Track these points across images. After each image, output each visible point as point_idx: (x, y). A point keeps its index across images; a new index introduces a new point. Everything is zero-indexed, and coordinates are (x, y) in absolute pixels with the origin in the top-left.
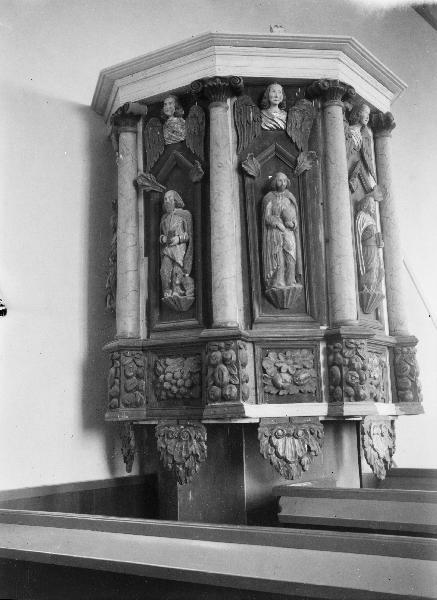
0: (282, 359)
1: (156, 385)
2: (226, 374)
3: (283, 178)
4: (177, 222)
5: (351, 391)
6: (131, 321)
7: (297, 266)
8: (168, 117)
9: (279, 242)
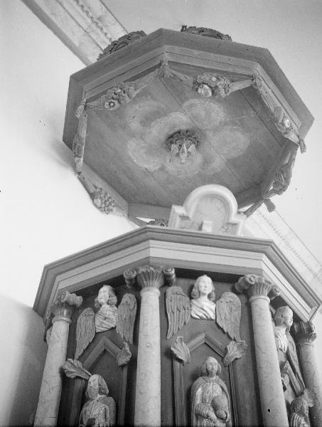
3: (213, 363)
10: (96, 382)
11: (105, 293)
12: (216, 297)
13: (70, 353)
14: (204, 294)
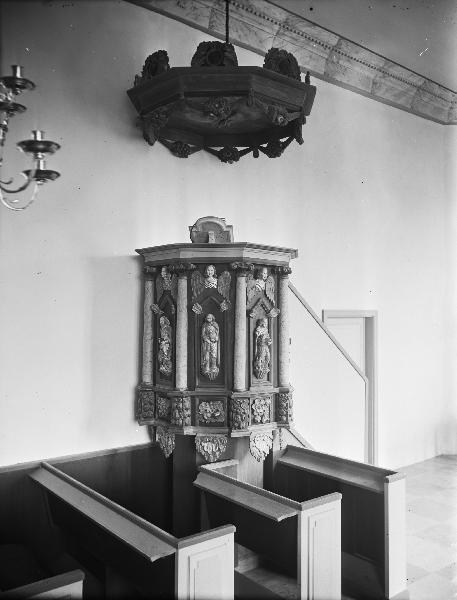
3: (210, 317)
5: (236, 425)
6: (148, 379)
12: (218, 275)
13: (155, 302)
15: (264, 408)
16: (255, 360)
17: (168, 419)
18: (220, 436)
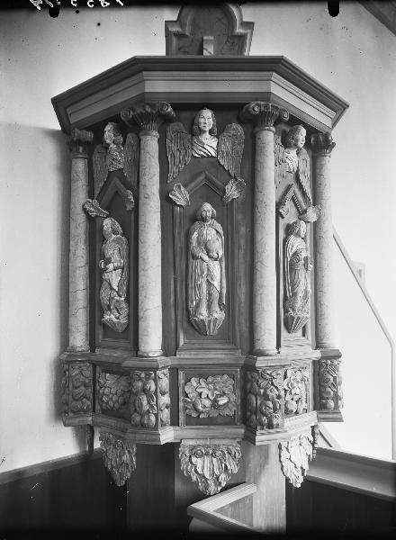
0: (203, 384)
1: (95, 396)
2: (145, 402)
3: (208, 208)
4: (114, 253)
5: (264, 419)
6: (79, 340)
7: (221, 294)
8: (109, 145)
9: (202, 272)
10: (109, 225)
11: (109, 133)
12: (218, 132)
13: (91, 195)
14: (205, 132)
15: (302, 388)
16: (285, 298)
17: (125, 413)
18: (225, 442)
